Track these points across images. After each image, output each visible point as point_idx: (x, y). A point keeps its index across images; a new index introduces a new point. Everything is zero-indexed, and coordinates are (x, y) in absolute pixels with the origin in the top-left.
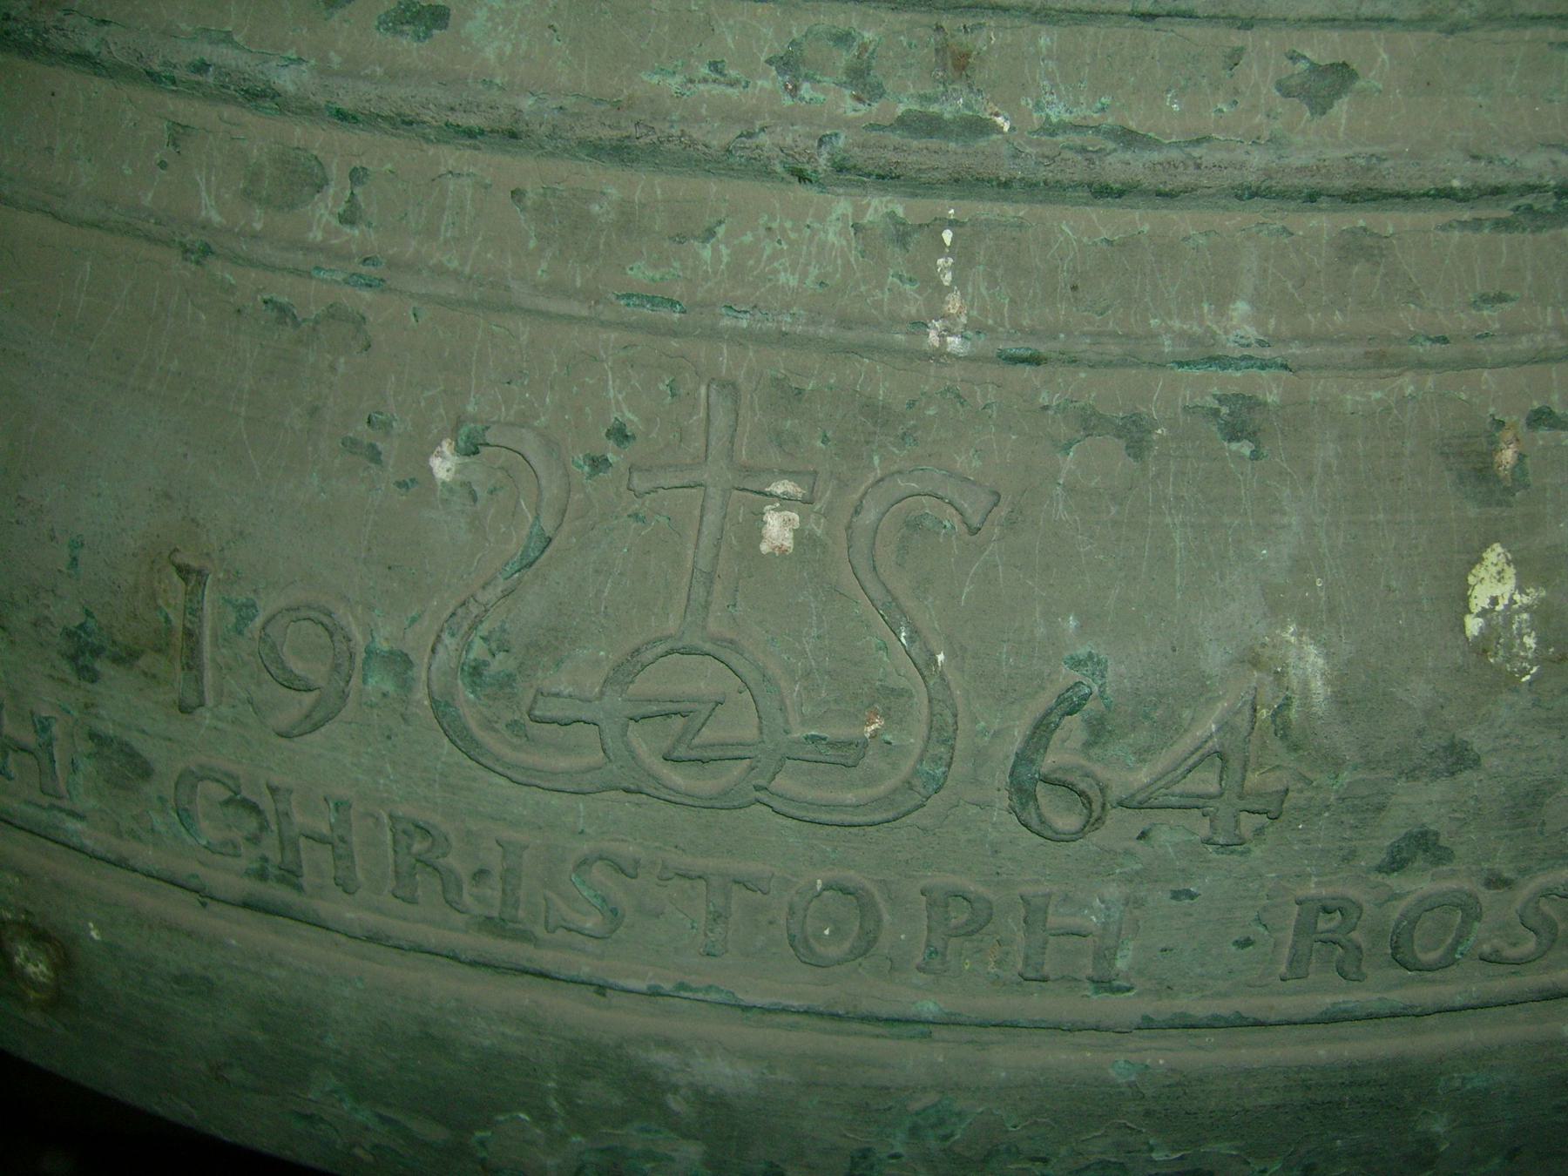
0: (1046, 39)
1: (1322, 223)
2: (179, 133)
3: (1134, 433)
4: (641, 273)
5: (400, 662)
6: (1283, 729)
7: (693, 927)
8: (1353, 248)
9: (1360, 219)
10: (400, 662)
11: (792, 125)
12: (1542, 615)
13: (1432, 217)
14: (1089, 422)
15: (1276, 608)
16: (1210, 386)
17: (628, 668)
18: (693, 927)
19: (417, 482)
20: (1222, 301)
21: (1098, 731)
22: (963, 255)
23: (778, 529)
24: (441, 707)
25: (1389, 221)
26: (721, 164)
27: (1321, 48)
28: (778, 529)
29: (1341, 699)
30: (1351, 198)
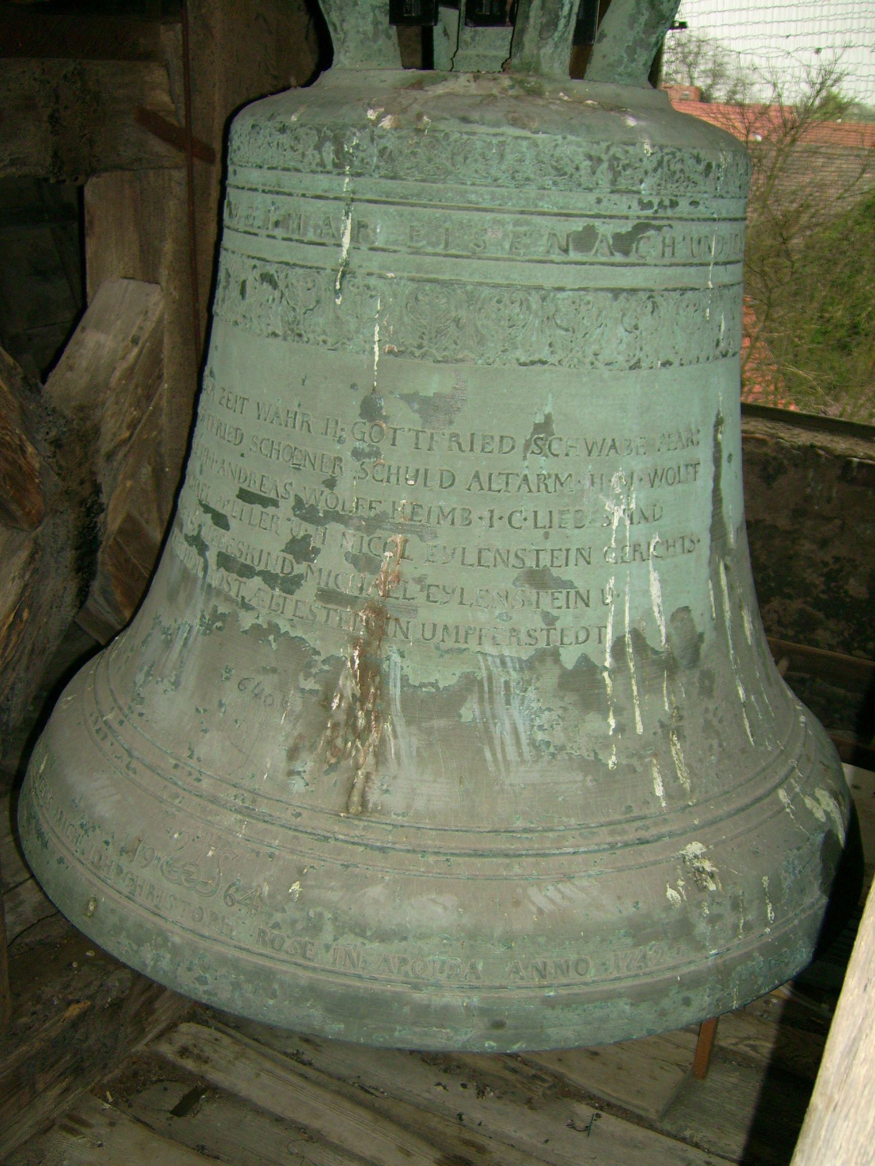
0: (266, 801)
1: (291, 833)
2: (165, 787)
3: (258, 853)
4: (209, 818)
5: (159, 859)
6: (260, 897)
7: (414, 154)
8: (295, 837)
9: (297, 834)
10: (159, 859)
11: (339, 854)
12: (300, 893)
13: (306, 836)
14: (253, 851)
15: (265, 880)
16: (269, 850)
17: (185, 865)
18: (414, 154)
19: (172, 837)
20: (275, 840)
21: (237, 890)
22: (247, 825)
23: (210, 853)
24: (162, 866)
25: (300, 835)
26: (224, 806)
27: (298, 810)
28: (210, 853)
29: (269, 895)
30: (295, 830)
